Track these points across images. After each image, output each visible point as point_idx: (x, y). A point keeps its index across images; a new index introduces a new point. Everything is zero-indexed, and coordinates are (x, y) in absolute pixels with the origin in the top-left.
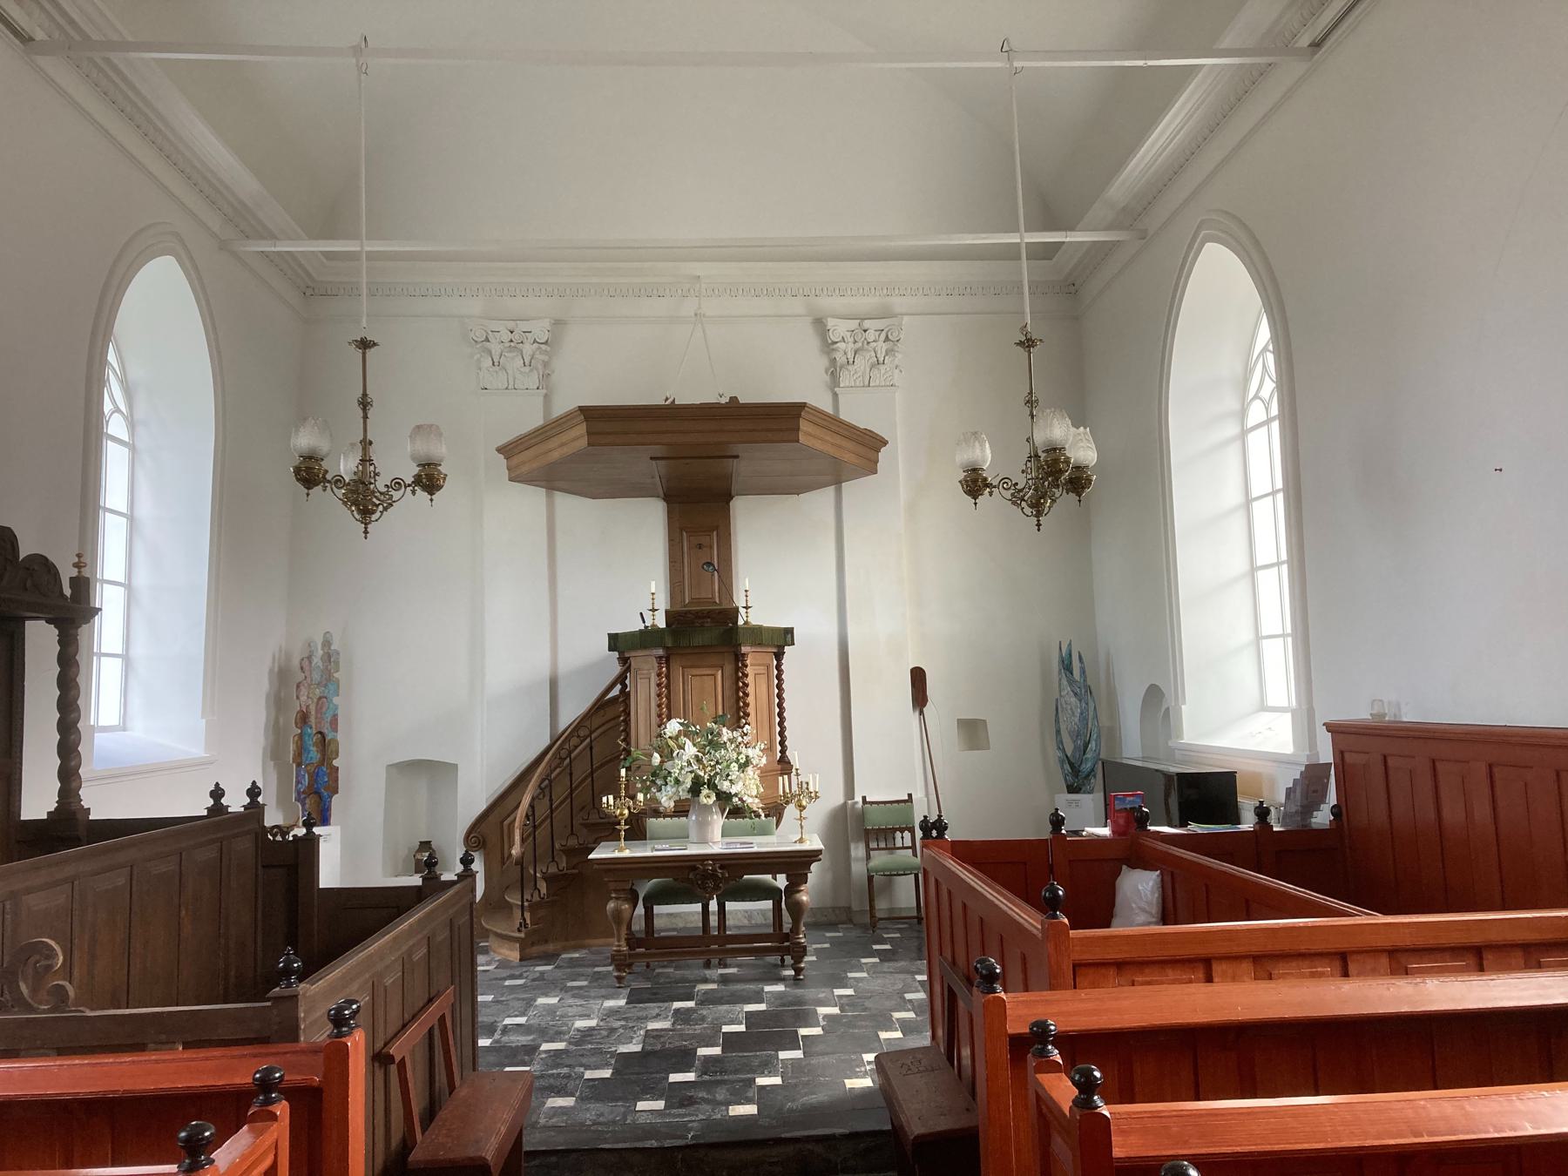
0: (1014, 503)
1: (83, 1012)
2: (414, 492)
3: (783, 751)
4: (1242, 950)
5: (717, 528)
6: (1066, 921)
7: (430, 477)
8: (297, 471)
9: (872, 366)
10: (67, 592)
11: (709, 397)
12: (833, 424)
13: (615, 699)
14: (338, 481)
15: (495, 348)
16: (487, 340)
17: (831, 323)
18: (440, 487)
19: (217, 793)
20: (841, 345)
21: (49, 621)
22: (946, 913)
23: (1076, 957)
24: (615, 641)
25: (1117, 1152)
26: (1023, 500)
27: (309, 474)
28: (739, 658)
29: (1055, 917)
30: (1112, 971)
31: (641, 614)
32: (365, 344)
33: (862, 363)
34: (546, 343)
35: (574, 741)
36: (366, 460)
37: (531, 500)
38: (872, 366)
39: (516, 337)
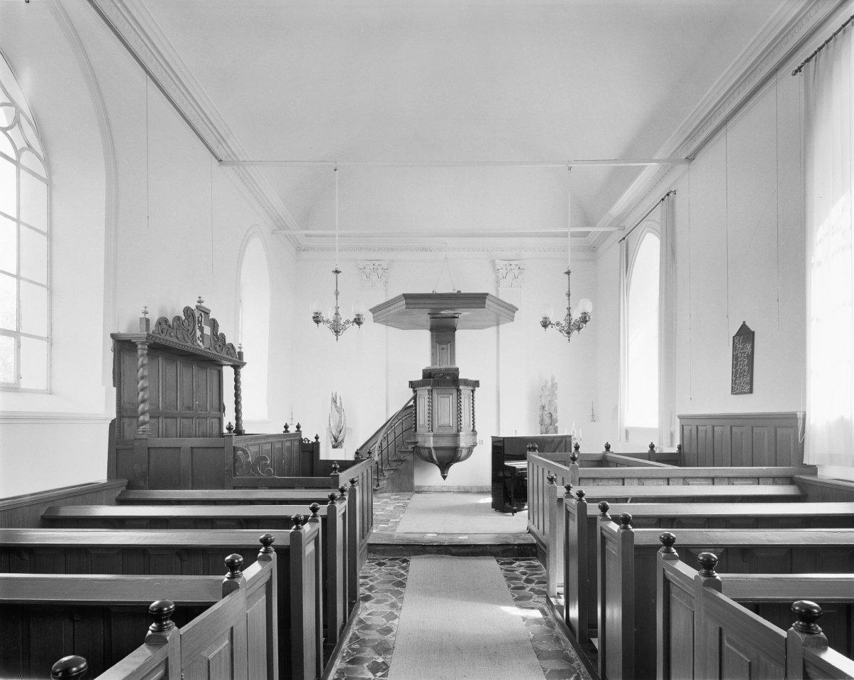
3: (474, 428)
4: (635, 476)
7: (359, 319)
8: (314, 317)
9: (513, 280)
11: (451, 291)
13: (411, 406)
14: (328, 321)
18: (362, 323)
19: (286, 427)
21: (232, 366)
22: (541, 513)
23: (581, 476)
24: (413, 385)
25: (588, 514)
27: (317, 319)
30: (592, 481)
31: (745, 336)
32: (337, 272)
33: (510, 276)
35: (396, 421)
37: (382, 327)
38: (513, 280)
39: (375, 267)
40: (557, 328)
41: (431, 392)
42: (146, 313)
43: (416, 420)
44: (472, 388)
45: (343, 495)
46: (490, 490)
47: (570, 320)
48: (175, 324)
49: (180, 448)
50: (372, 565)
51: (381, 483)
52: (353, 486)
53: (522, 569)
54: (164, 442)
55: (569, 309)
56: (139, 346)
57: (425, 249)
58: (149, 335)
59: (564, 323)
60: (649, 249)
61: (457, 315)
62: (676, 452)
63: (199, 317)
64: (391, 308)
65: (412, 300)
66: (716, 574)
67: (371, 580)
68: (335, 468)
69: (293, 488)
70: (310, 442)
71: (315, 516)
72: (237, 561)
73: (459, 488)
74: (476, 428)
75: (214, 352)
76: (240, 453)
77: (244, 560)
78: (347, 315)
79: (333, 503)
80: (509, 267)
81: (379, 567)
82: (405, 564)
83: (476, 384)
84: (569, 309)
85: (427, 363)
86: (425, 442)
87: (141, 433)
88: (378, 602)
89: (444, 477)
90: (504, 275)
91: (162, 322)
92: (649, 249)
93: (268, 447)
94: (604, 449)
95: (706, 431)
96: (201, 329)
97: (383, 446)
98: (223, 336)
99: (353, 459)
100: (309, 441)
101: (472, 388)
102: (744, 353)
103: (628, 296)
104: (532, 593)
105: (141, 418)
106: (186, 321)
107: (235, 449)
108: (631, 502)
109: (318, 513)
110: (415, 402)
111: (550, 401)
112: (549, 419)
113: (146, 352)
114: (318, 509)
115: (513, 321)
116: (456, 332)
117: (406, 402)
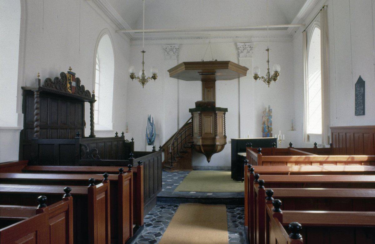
0: (264, 81)
1: (24, 219)
2: (151, 79)
5: (213, 87)
6: (261, 154)
7: (155, 76)
8: (130, 76)
10: (92, 97)
11: (211, 60)
12: (238, 66)
13: (190, 123)
14: (138, 78)
15: (168, 50)
16: (166, 48)
17: (238, 44)
18: (156, 79)
19: (117, 134)
20: (240, 48)
21: (89, 102)
23: (263, 160)
24: (191, 111)
26: (266, 81)
28: (216, 114)
29: (259, 153)
31: (361, 83)
32: (143, 52)
33: (245, 51)
34: (178, 49)
36: (143, 74)
37: (175, 80)
38: (247, 53)
39: (172, 48)
40: (263, 80)
41: (200, 115)
42: (70, 69)
43: (193, 130)
44: (224, 112)
45: (130, 170)
46: (230, 168)
47: (269, 75)
48: (55, 81)
49: (54, 144)
50: (158, 208)
51: (173, 164)
52: (139, 165)
53: (238, 212)
54: (45, 141)
55: (268, 69)
56: (35, 93)
57: (199, 38)
58: (40, 87)
59: (266, 77)
60: (316, 35)
61: (214, 73)
62: (313, 147)
63: (69, 77)
64: (178, 70)
65: (189, 65)
66: (281, 211)
67: (155, 216)
68: (131, 156)
69: (109, 166)
70: (129, 142)
71: (106, 180)
72: (43, 199)
73: (217, 167)
74: (226, 134)
75: (78, 95)
76: (83, 147)
77: (47, 199)
78: (148, 74)
79: (121, 173)
80: (244, 47)
81: (161, 209)
82: (175, 208)
83: (226, 110)
84: (268, 69)
85: (199, 98)
86: (197, 142)
87: (35, 137)
88: (155, 227)
89: (209, 161)
90: (242, 51)
91: (48, 81)
92: (316, 35)
93: (103, 144)
94: (289, 146)
95: (343, 136)
96: (70, 83)
97: (175, 145)
98: (83, 87)
99: (152, 151)
100: (128, 141)
101: (224, 112)
102: (360, 93)
103: (307, 63)
104: (239, 224)
105: (36, 129)
106: (62, 79)
107: (81, 145)
108: (290, 175)
109: (108, 178)
110: (192, 120)
111: (268, 119)
112: (267, 128)
113: (39, 96)
114: (108, 176)
115: (246, 75)
116: (216, 82)
117: (187, 121)
